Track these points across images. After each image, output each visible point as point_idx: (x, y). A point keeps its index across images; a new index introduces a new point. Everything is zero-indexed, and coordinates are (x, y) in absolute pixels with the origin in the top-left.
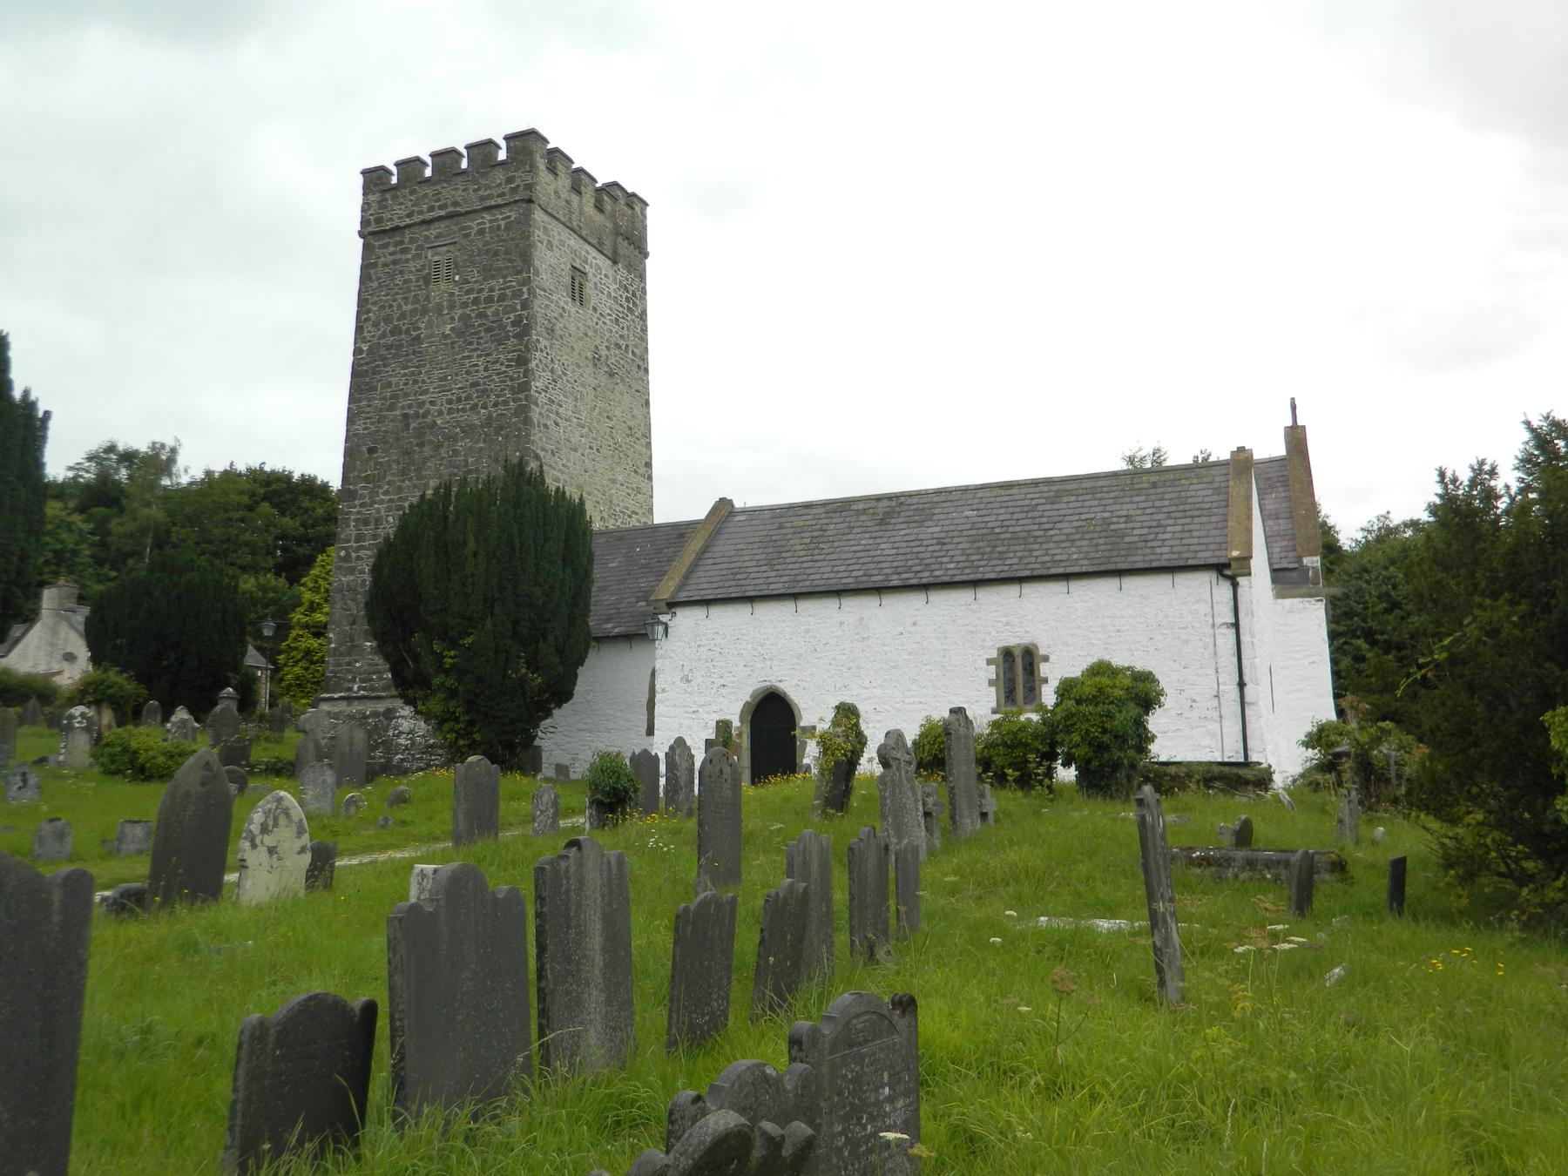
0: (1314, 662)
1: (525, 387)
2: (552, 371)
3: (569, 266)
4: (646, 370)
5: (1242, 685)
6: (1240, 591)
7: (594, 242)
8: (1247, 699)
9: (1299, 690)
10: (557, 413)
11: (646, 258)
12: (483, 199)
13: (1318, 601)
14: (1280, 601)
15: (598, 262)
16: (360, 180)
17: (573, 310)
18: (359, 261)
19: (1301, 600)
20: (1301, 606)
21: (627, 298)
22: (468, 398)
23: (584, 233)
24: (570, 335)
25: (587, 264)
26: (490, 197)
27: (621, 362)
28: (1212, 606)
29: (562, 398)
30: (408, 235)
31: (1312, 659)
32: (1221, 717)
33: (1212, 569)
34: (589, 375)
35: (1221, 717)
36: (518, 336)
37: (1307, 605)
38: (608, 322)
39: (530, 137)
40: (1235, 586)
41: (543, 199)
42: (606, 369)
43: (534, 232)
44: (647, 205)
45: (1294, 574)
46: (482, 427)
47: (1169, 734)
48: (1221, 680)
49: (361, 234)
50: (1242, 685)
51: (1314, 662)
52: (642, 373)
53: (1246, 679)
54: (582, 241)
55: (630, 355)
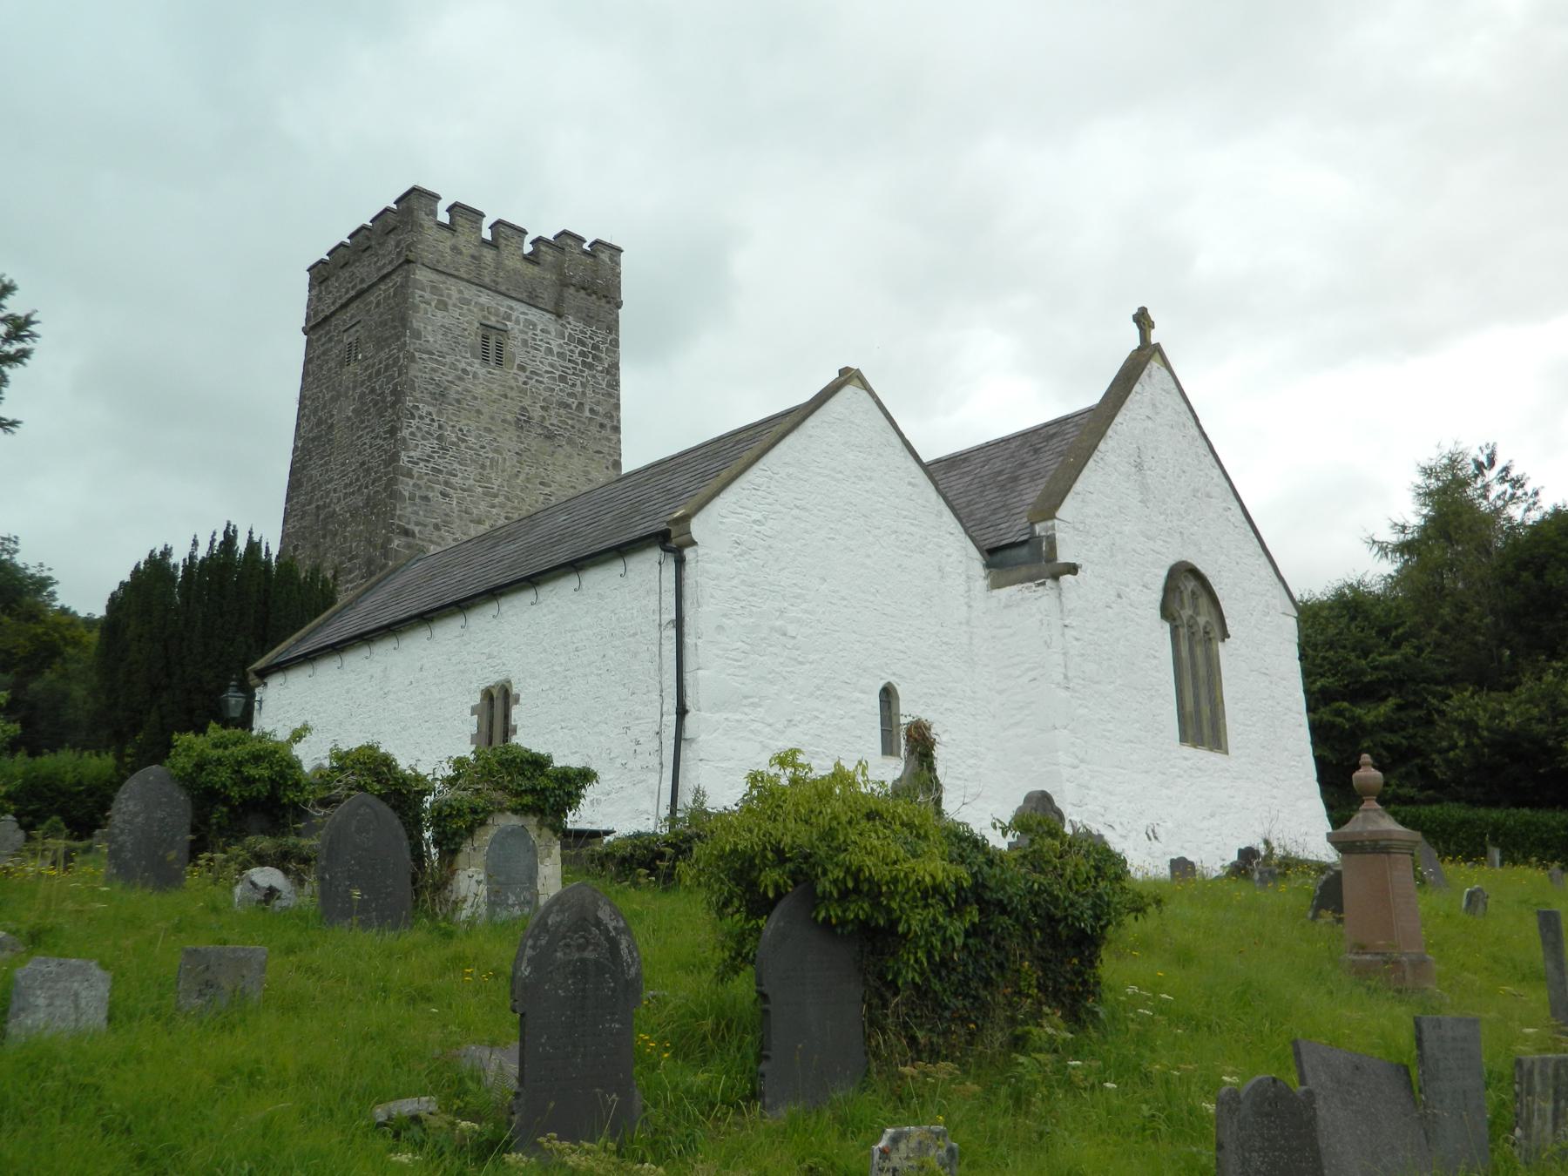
0: (1035, 679)
1: (395, 457)
2: (440, 438)
3: (477, 325)
4: (617, 429)
5: (682, 712)
6: (690, 570)
7: (524, 296)
8: (688, 734)
9: (1017, 724)
10: (447, 483)
11: (619, 307)
12: (380, 269)
13: (1039, 585)
14: (996, 592)
15: (530, 317)
16: (307, 276)
17: (482, 371)
18: (303, 358)
19: (1020, 586)
20: (1019, 596)
21: (582, 354)
22: (357, 480)
23: (503, 289)
24: (476, 398)
25: (510, 320)
26: (384, 266)
27: (570, 422)
28: (660, 598)
29: (456, 466)
30: (334, 321)
31: (1032, 674)
32: (661, 764)
33: (649, 546)
34: (509, 440)
35: (661, 764)
36: (393, 405)
37: (1027, 594)
38: (545, 380)
39: (412, 196)
40: (680, 563)
41: (428, 257)
42: (540, 431)
43: (413, 293)
44: (620, 251)
45: (1024, 551)
46: (363, 508)
47: (613, 795)
48: (665, 709)
49: (305, 331)
50: (682, 712)
51: (1035, 679)
52: (607, 433)
53: (689, 703)
54: (501, 297)
55: (587, 414)
